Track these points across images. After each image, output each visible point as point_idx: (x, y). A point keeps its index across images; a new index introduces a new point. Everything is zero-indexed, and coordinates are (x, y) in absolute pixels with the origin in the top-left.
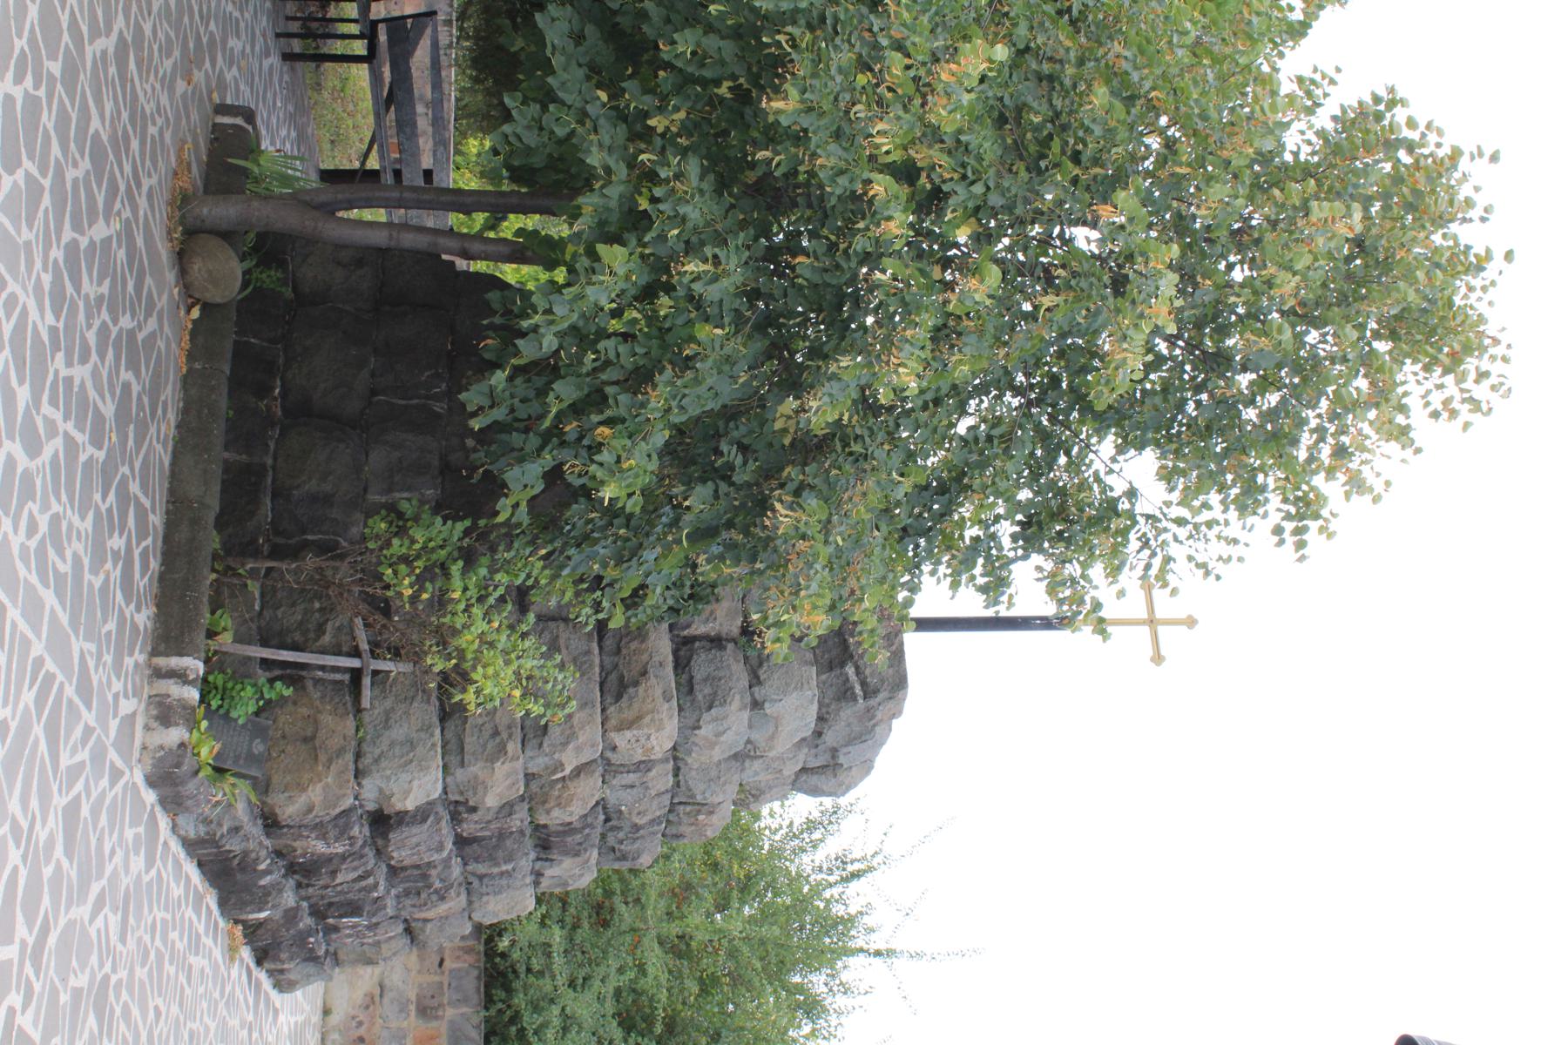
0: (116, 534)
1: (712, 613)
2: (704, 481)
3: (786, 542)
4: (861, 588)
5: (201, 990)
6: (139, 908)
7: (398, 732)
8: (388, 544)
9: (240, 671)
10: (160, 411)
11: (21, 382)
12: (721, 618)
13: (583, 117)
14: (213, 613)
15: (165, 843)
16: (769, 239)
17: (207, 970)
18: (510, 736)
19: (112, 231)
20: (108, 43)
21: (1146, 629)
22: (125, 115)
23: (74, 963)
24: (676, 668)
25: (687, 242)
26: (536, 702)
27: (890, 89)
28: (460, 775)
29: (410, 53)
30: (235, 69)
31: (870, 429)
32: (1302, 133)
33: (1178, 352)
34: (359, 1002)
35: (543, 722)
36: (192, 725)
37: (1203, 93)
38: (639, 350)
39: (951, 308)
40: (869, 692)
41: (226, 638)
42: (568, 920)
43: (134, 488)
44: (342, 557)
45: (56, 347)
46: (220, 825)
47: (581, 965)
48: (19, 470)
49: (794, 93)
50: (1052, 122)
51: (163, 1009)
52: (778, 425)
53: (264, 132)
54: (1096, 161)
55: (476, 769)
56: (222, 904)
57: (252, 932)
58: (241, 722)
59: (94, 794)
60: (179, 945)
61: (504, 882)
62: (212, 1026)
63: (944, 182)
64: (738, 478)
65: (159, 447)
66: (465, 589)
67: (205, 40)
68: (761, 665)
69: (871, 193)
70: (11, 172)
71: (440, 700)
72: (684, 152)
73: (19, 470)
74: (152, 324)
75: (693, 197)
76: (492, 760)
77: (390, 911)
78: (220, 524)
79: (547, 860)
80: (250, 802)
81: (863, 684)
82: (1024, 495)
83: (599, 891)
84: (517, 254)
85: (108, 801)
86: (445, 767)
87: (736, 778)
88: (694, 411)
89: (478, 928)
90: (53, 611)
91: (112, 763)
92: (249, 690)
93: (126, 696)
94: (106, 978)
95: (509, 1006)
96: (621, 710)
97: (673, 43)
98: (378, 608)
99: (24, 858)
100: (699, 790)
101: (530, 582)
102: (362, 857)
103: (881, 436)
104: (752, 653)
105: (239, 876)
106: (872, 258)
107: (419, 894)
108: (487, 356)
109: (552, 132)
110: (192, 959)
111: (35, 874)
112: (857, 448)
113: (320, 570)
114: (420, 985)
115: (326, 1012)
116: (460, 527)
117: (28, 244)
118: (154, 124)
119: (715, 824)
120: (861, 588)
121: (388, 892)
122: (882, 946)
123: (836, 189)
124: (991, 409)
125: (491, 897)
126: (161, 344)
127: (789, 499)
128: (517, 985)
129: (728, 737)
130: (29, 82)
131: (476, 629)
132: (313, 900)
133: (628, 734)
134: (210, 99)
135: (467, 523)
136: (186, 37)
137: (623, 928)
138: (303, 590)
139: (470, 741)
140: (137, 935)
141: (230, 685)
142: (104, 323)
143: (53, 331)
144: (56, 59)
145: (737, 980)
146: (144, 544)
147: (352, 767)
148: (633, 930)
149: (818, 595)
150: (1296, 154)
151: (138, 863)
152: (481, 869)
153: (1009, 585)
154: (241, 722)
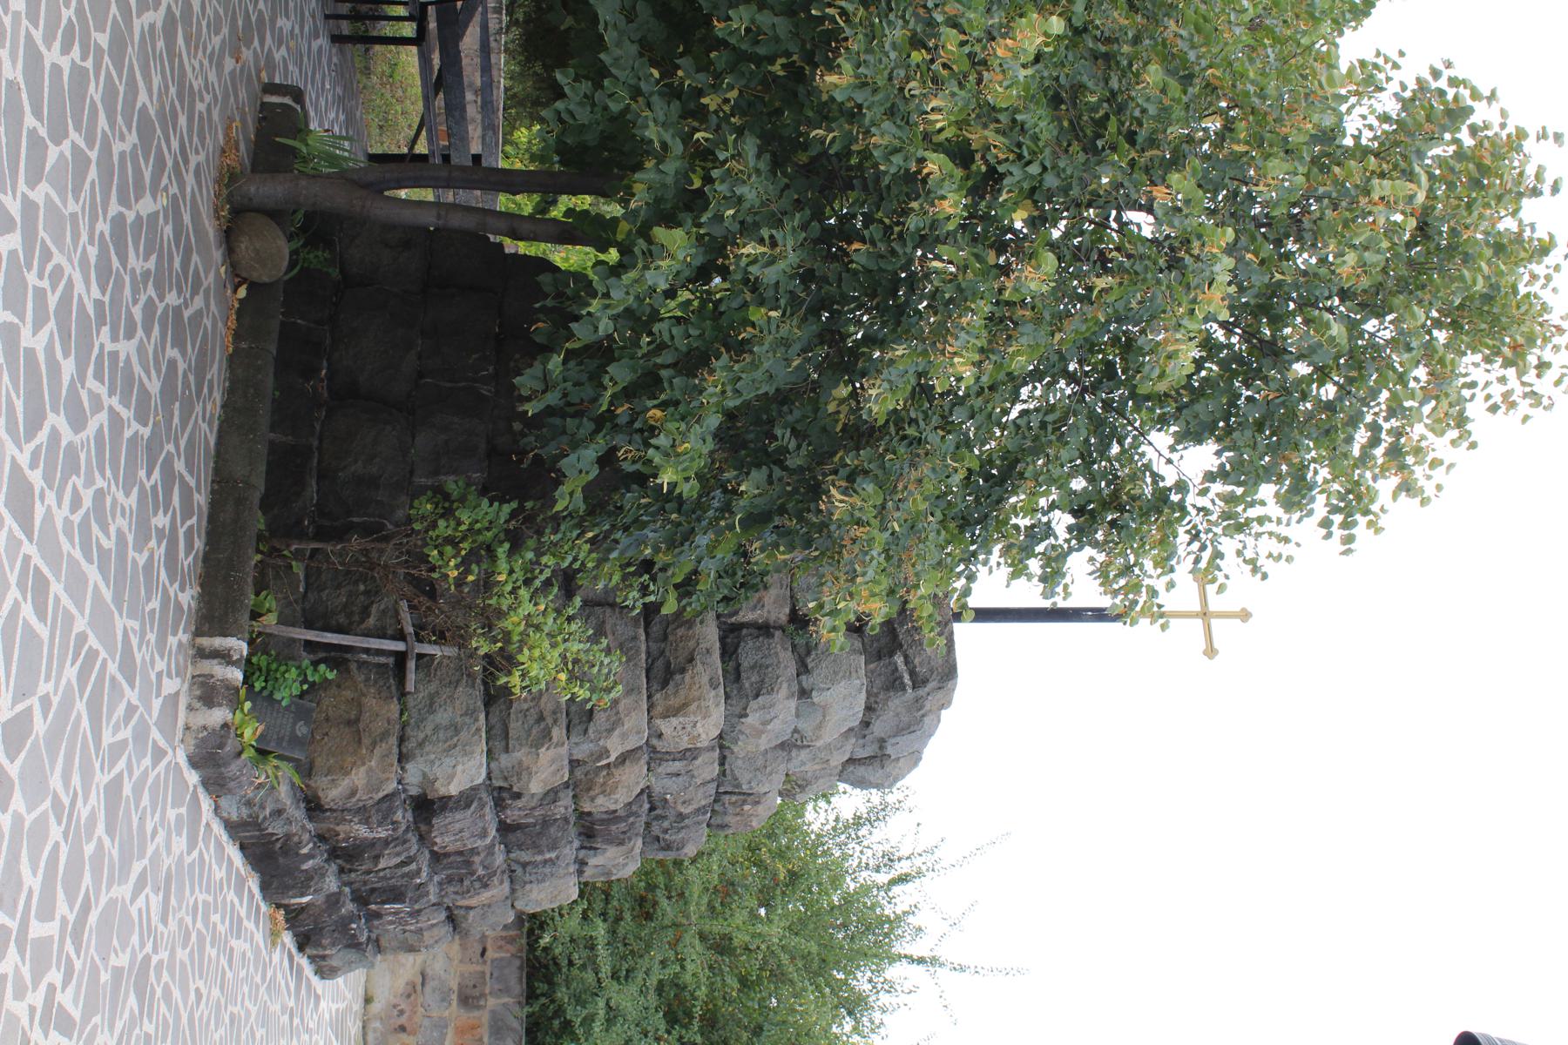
0: (161, 512)
1: (760, 600)
2: (758, 466)
3: (839, 527)
4: (917, 575)
5: (243, 974)
6: (181, 889)
7: (443, 716)
8: (434, 526)
9: (285, 652)
10: (206, 390)
11: (66, 355)
12: (770, 606)
13: (636, 93)
14: (257, 594)
15: (208, 824)
16: (821, 221)
17: (249, 954)
18: (555, 721)
19: (159, 207)
20: (156, 17)
21: (1199, 622)
22: (173, 90)
23: (115, 942)
24: (723, 655)
25: (742, 223)
26: (581, 687)
27: (945, 66)
28: (505, 761)
29: (460, 36)
30: (283, 48)
31: (925, 412)
32: (1364, 117)
33: (1235, 340)
34: (401, 991)
35: (588, 707)
36: (235, 705)
37: (1263, 74)
38: (694, 332)
39: (1007, 295)
40: (918, 682)
41: (271, 620)
42: (611, 913)
43: (179, 466)
44: (386, 539)
45: (101, 321)
46: (263, 807)
47: (624, 958)
48: (64, 443)
49: (847, 67)
50: (1108, 101)
51: (204, 991)
52: (831, 408)
53: (312, 114)
54: (1153, 142)
55: (520, 754)
56: (264, 887)
57: (294, 917)
58: (284, 703)
59: (137, 773)
60: (221, 928)
61: (547, 870)
62: (254, 1010)
63: (999, 163)
64: (794, 462)
65: (205, 426)
66: (511, 572)
67: (253, 19)
68: (808, 653)
69: (925, 171)
70: (58, 143)
71: (485, 683)
72: (740, 131)
73: (64, 443)
74: (198, 302)
75: (749, 177)
76: (537, 745)
77: (433, 898)
78: (265, 505)
79: (591, 848)
80: (293, 784)
81: (912, 673)
82: (1078, 484)
83: (642, 884)
84: (566, 234)
85: (150, 781)
86: (489, 752)
87: (782, 768)
88: (748, 395)
89: (520, 918)
90: (96, 585)
91: (154, 742)
92: (294, 673)
93: (169, 676)
94: (147, 958)
95: (553, 1001)
96: (667, 697)
97: (729, 19)
98: (424, 592)
99: (66, 834)
100: (744, 777)
101: (577, 565)
102: (405, 842)
103: (935, 421)
104: (800, 641)
105: (281, 860)
106: (928, 239)
107: (461, 881)
108: (538, 339)
109: (606, 108)
110: (234, 943)
111: (76, 851)
112: (911, 431)
113: (365, 552)
114: (462, 975)
115: (368, 1000)
116: (507, 509)
117: (74, 216)
118: (202, 100)
119: (759, 817)
120: (917, 575)
121: (431, 879)
122: (926, 954)
123: (890, 168)
124: (1044, 396)
125: (534, 885)
126: (207, 322)
127: (844, 484)
128: (559, 979)
129: (775, 726)
130: (76, 52)
131: (525, 611)
132: (355, 886)
133: (674, 721)
134: (259, 78)
135: (514, 505)
136: (234, 12)
137: (666, 922)
138: (348, 572)
139: (515, 727)
140: (178, 916)
141: (274, 666)
142: (150, 299)
143: (99, 304)
144: (104, 31)
145: (779, 976)
146: (189, 523)
147: (395, 750)
148: (676, 925)
149: (874, 581)
150: (1357, 138)
151: (180, 843)
152: (525, 856)
153: (1064, 575)
154: (284, 703)
